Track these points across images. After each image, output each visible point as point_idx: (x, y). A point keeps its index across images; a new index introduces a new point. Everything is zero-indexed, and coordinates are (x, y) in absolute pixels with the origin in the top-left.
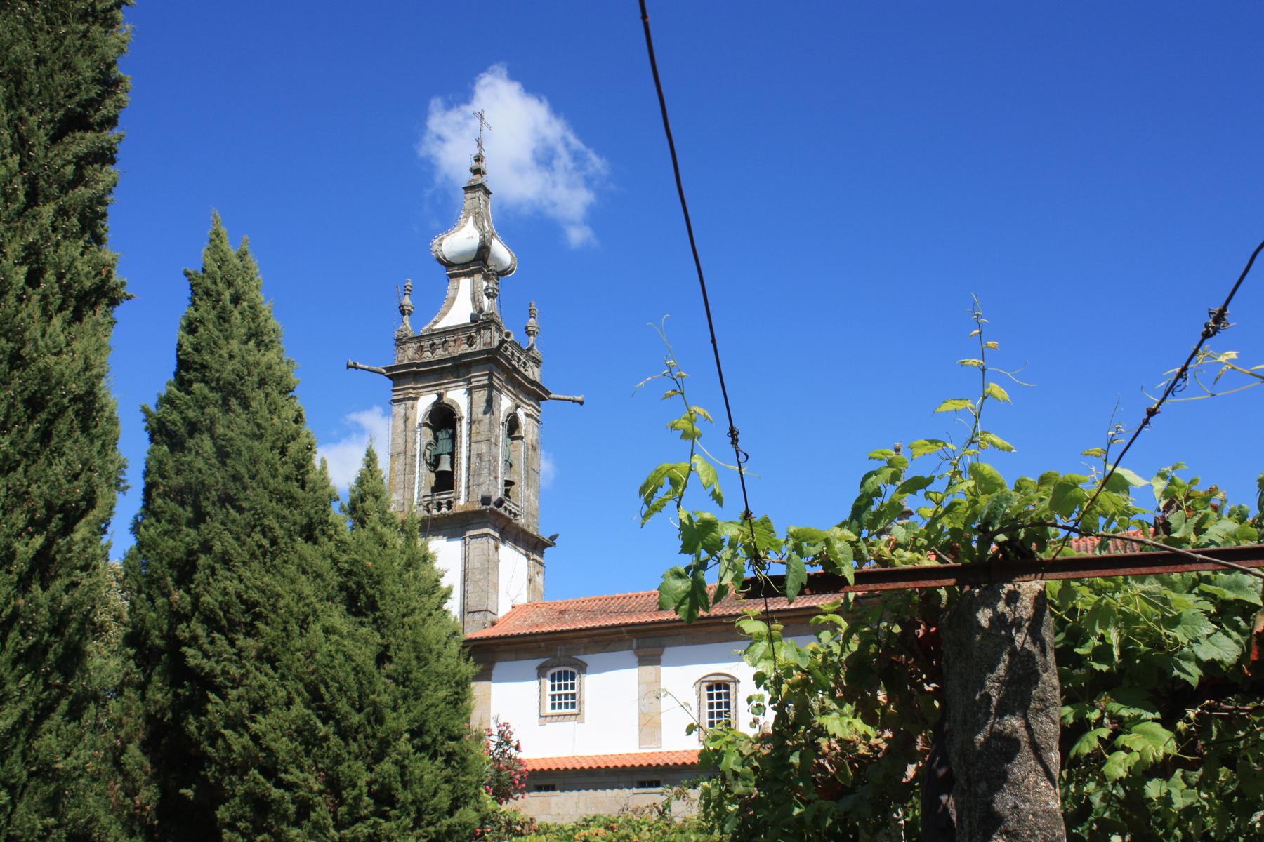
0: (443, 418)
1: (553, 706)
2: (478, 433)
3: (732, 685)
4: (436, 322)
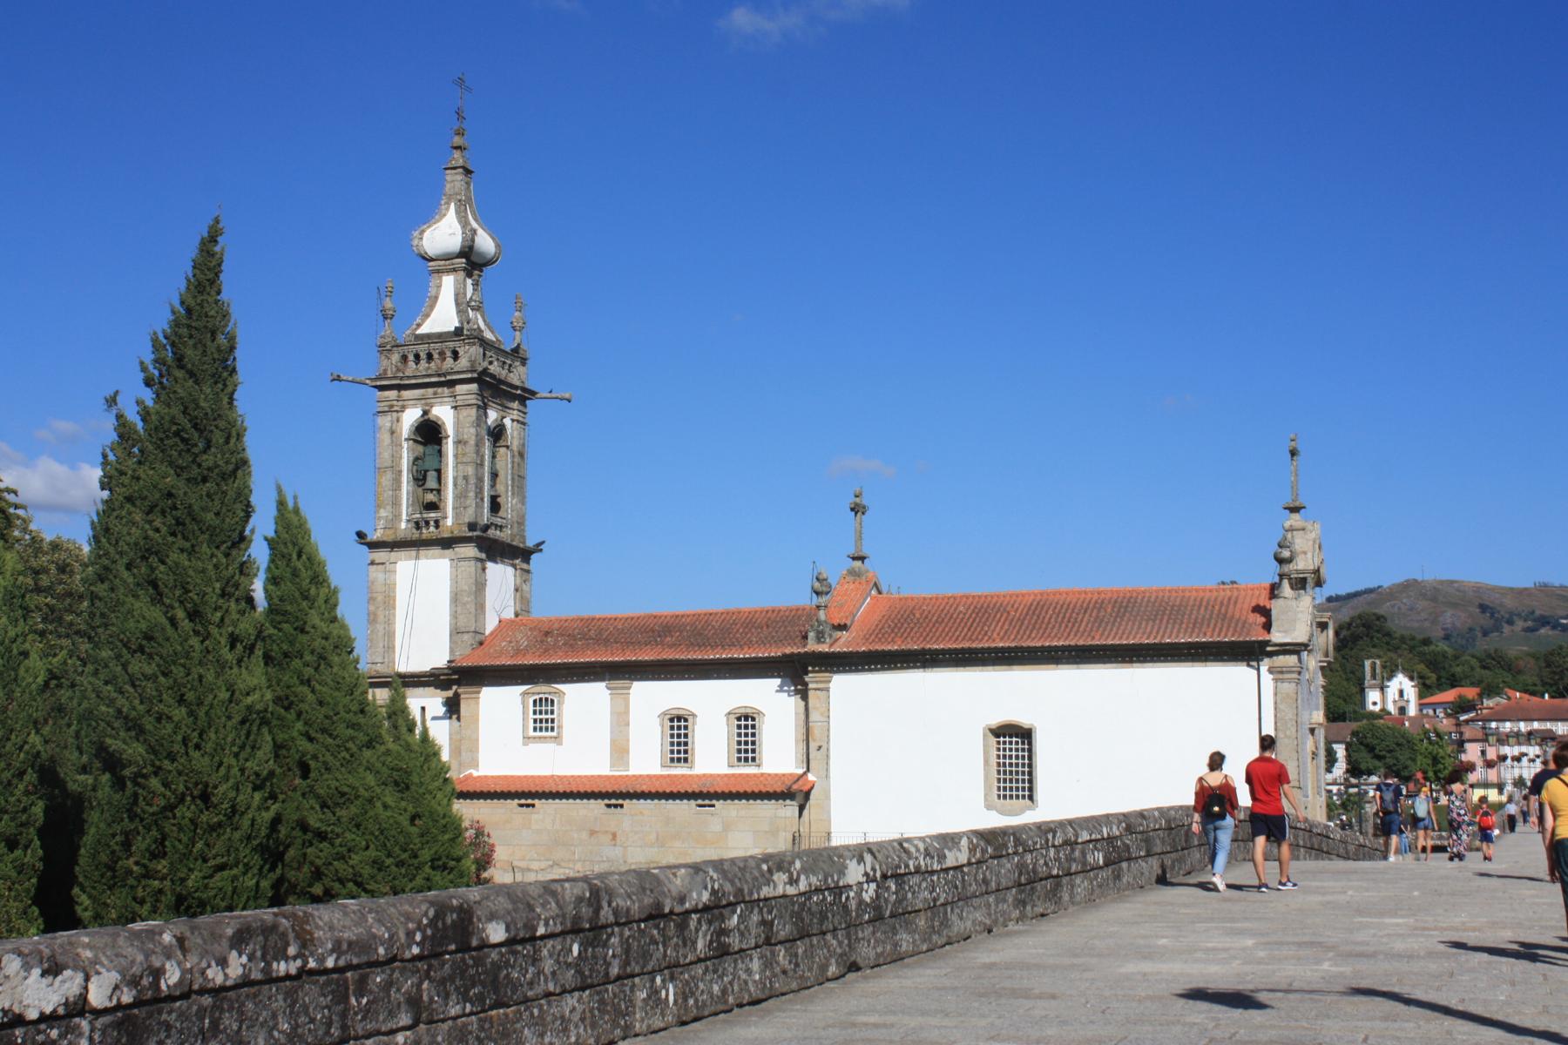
0: (429, 433)
1: (535, 729)
2: (464, 455)
3: (690, 719)
4: (419, 325)
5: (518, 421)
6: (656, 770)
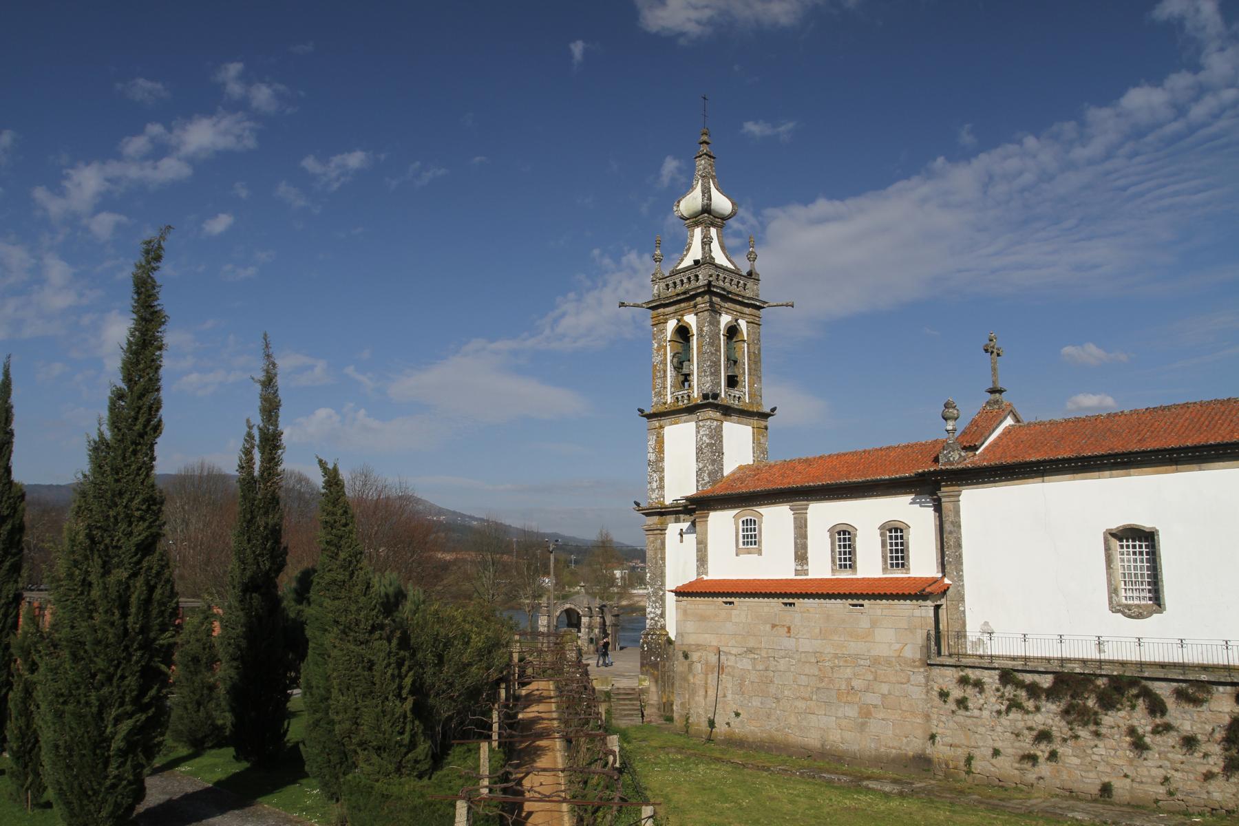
0: (683, 333)
5: (752, 323)
6: (878, 574)
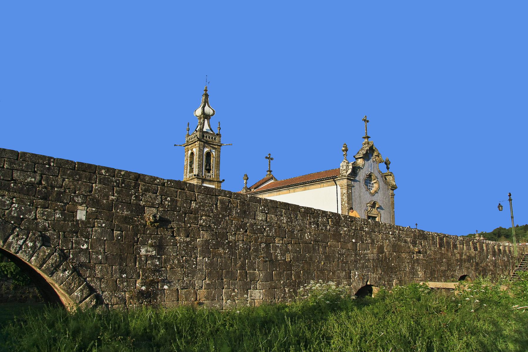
0: (192, 154)
